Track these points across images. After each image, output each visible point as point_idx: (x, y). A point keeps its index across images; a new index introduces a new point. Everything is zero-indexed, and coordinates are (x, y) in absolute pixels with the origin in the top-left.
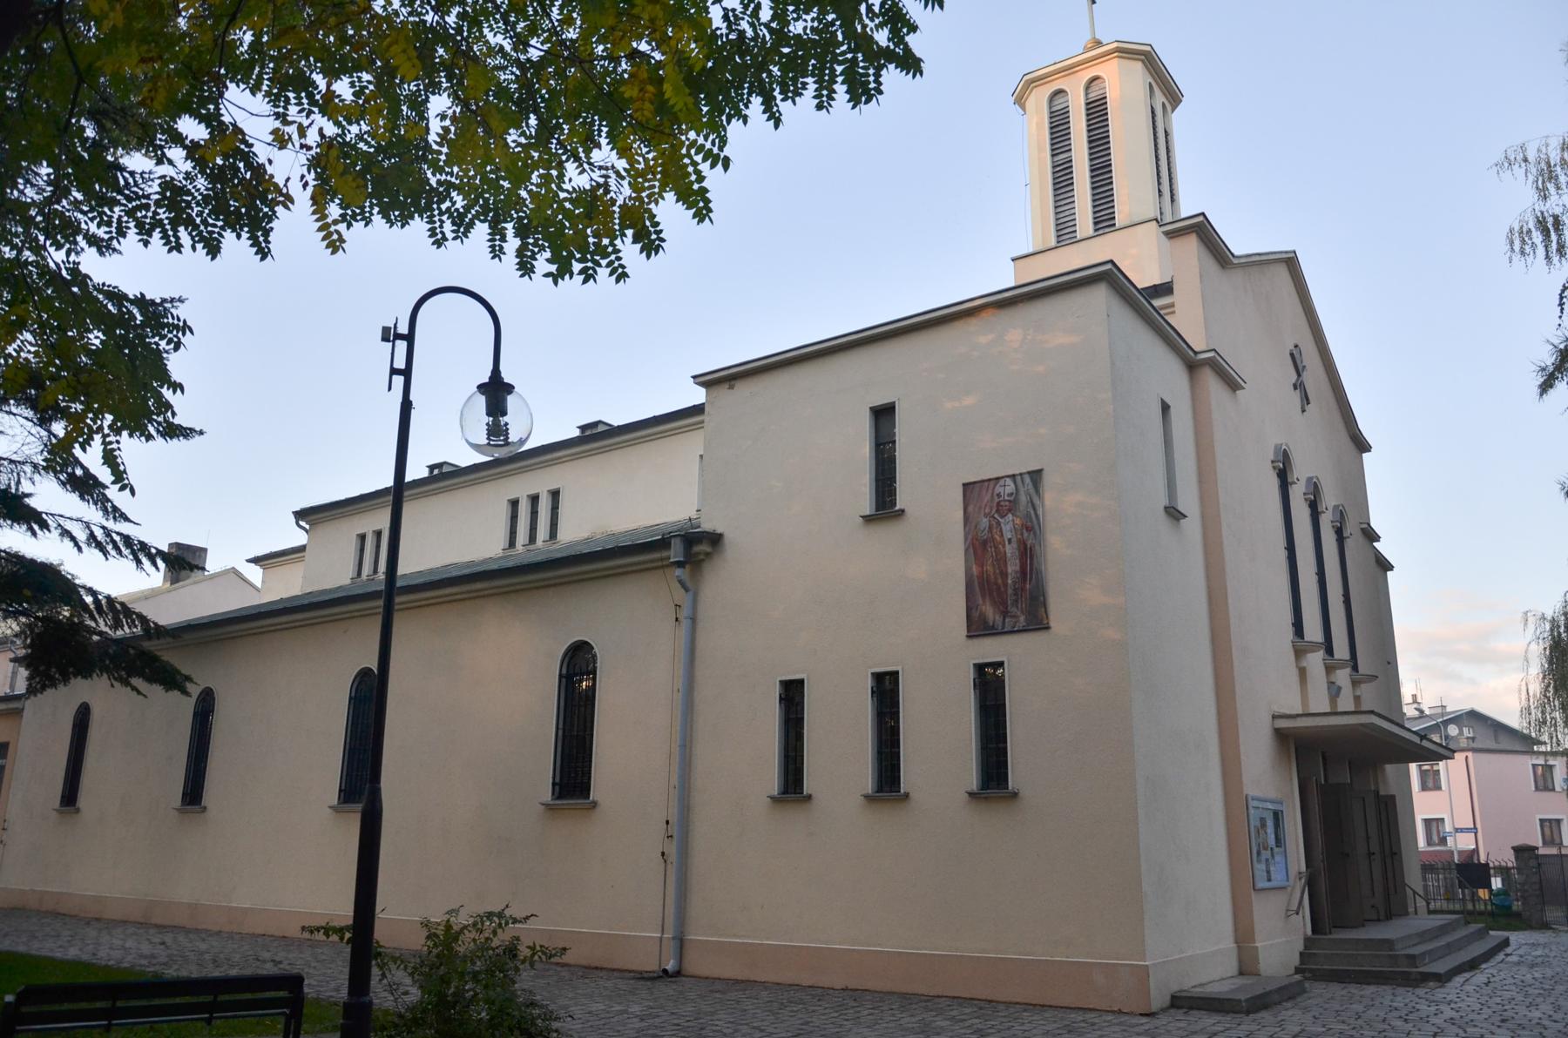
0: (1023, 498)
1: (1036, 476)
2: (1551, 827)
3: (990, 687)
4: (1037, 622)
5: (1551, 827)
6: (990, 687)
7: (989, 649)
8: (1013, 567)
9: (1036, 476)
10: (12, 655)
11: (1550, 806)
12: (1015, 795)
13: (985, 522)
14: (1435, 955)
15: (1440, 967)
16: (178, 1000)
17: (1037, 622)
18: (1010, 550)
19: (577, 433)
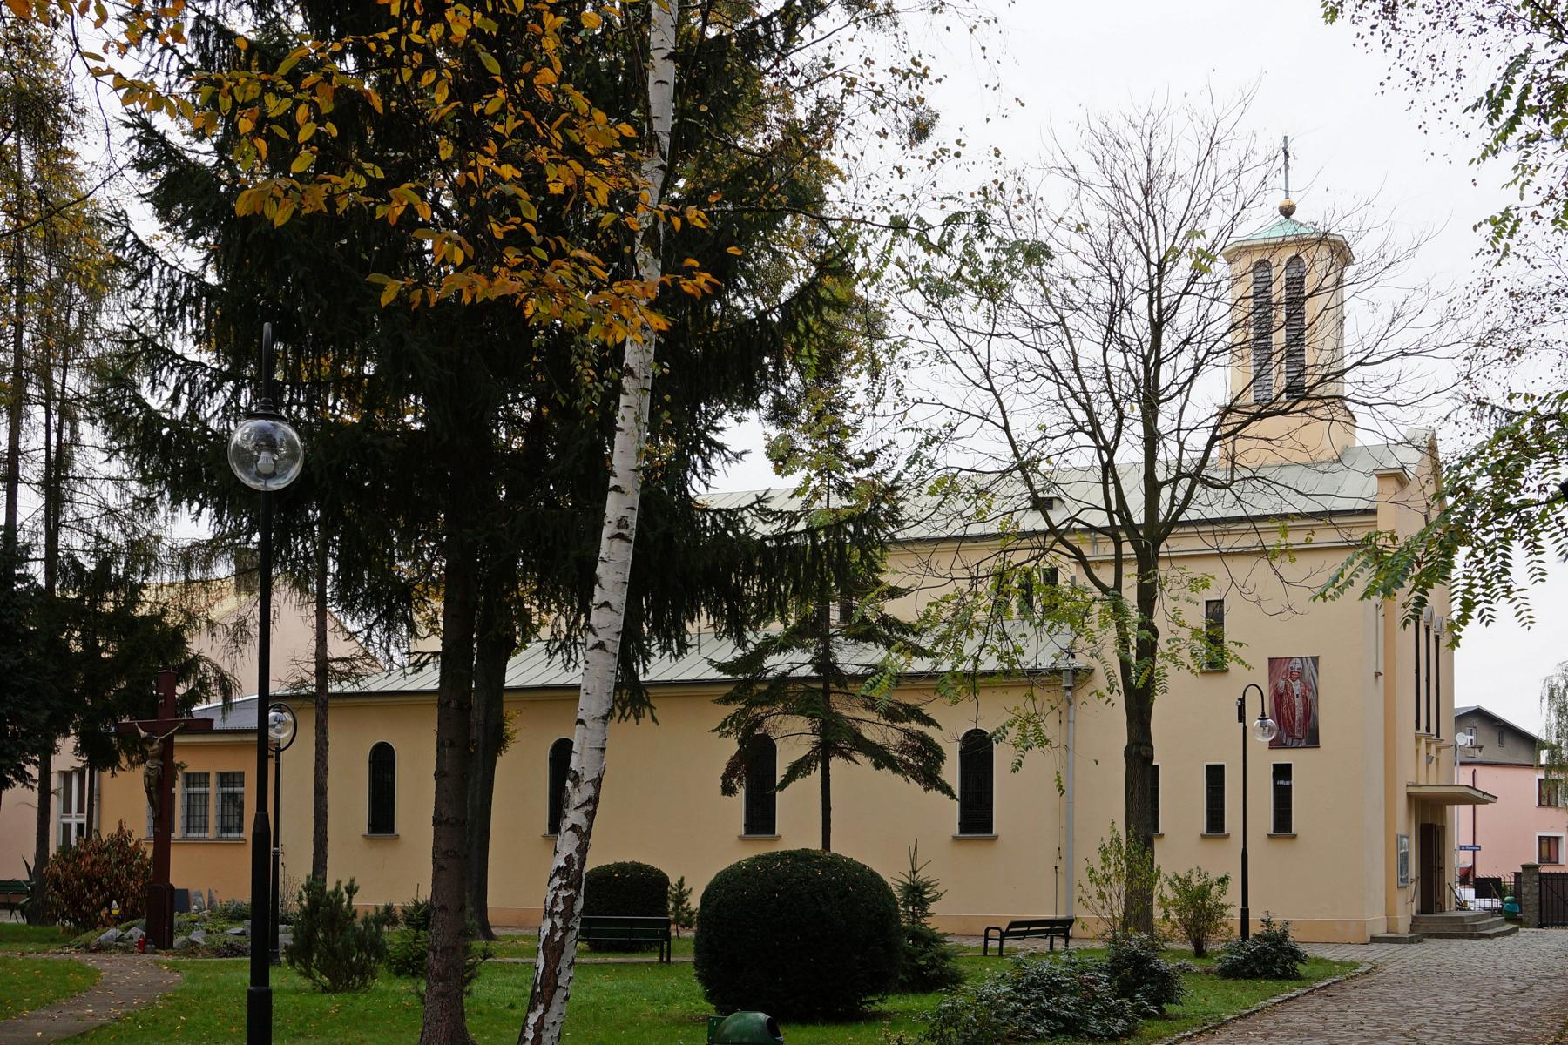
0: (1307, 672)
1: (1315, 660)
2: (1549, 845)
3: (1282, 771)
4: (1312, 739)
5: (1549, 845)
6: (1282, 771)
7: (1283, 757)
8: (1299, 713)
9: (1315, 660)
10: (232, 591)
11: (1551, 822)
12: (1295, 836)
13: (1282, 683)
14: (1489, 926)
15: (1491, 932)
16: (610, 959)
17: (1312, 740)
18: (1298, 701)
19: (859, 757)
